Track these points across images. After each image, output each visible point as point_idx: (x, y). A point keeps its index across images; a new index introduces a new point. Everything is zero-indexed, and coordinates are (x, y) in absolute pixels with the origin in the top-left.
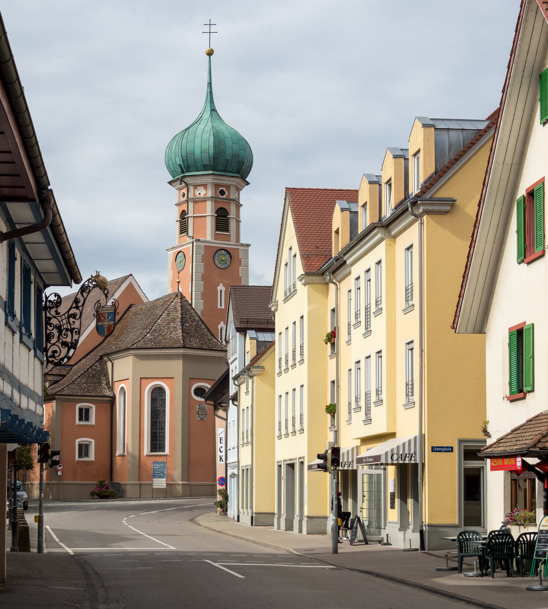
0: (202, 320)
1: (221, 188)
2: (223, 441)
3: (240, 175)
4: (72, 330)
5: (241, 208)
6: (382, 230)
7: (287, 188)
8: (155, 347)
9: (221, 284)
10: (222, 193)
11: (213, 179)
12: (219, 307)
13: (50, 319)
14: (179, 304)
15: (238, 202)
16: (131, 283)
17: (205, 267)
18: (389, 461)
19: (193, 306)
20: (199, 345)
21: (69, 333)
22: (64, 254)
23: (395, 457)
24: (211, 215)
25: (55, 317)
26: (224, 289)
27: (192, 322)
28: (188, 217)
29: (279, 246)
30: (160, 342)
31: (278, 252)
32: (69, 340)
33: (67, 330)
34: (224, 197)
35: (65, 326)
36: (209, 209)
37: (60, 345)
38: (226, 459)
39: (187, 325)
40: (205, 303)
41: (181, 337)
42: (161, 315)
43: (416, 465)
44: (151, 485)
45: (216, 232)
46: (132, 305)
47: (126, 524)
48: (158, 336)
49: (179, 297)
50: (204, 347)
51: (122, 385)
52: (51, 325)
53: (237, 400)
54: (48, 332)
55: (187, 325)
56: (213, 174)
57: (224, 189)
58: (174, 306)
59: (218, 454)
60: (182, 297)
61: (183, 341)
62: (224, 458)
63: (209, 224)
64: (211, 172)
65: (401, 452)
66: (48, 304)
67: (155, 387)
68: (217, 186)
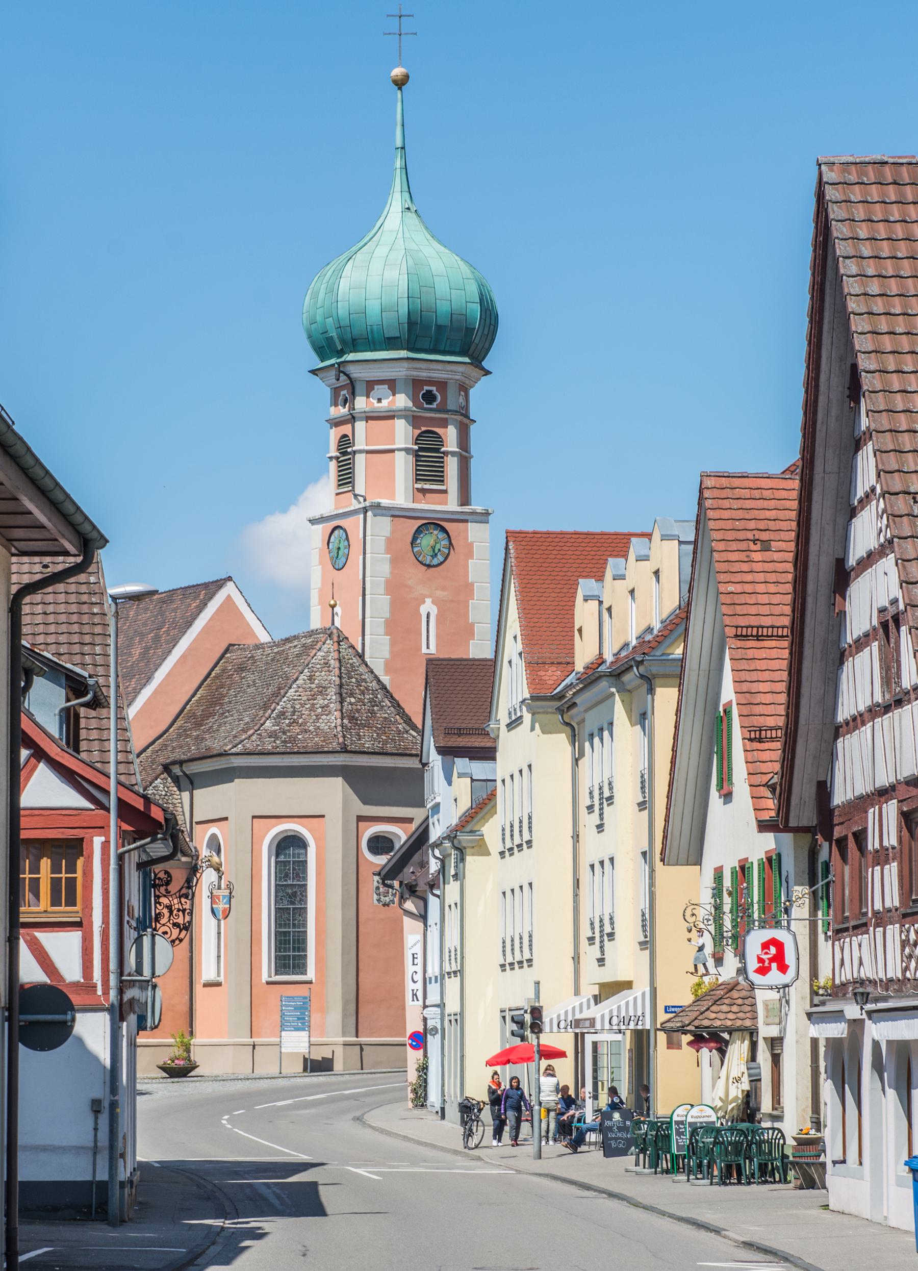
0: (384, 688)
1: (426, 388)
2: (419, 961)
3: (470, 357)
4: (184, 911)
5: (473, 428)
6: (612, 679)
7: (507, 532)
8: (282, 749)
9: (428, 601)
10: (429, 397)
11: (408, 369)
12: (424, 650)
13: (159, 897)
14: (336, 655)
15: (466, 416)
16: (229, 597)
17: (394, 562)
18: (607, 1026)
19: (367, 659)
20: (377, 746)
21: (181, 913)
22: (78, 527)
23: (615, 1021)
24: (407, 450)
25: (165, 896)
26: (434, 611)
27: (363, 693)
28: (355, 452)
29: (499, 626)
30: (293, 739)
31: (497, 636)
32: (180, 920)
33: (179, 910)
34: (434, 406)
35: (177, 906)
36: (402, 434)
37: (171, 926)
38: (425, 997)
39: (353, 700)
40: (393, 643)
41: (339, 729)
42: (297, 679)
43: (648, 1031)
44: (279, 1045)
45: (417, 486)
46: (230, 645)
47: (229, 1126)
48: (289, 725)
49: (336, 639)
50: (389, 748)
51: (214, 829)
52: (160, 904)
53: (439, 888)
54: (158, 911)
55: (353, 700)
56: (408, 359)
57: (434, 389)
58: (324, 658)
59: (410, 986)
60: (341, 639)
61: (344, 736)
62: (420, 995)
63: (403, 465)
64: (403, 354)
65: (623, 1014)
66: (157, 881)
67: (285, 835)
68: (416, 383)
